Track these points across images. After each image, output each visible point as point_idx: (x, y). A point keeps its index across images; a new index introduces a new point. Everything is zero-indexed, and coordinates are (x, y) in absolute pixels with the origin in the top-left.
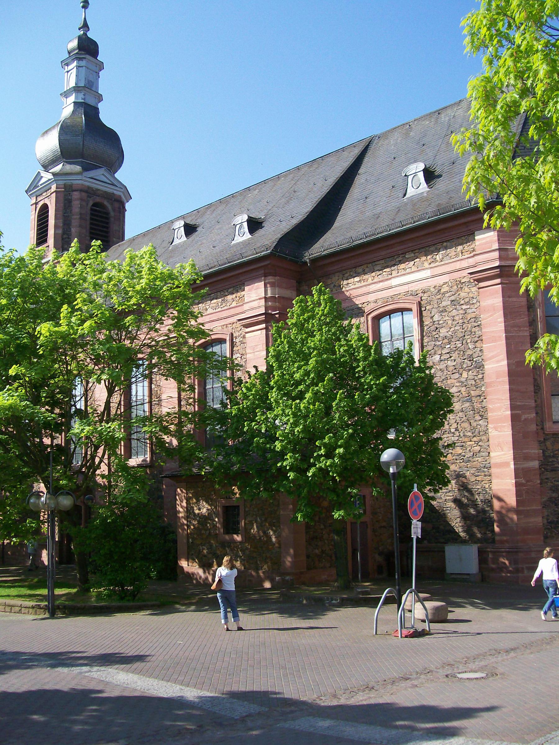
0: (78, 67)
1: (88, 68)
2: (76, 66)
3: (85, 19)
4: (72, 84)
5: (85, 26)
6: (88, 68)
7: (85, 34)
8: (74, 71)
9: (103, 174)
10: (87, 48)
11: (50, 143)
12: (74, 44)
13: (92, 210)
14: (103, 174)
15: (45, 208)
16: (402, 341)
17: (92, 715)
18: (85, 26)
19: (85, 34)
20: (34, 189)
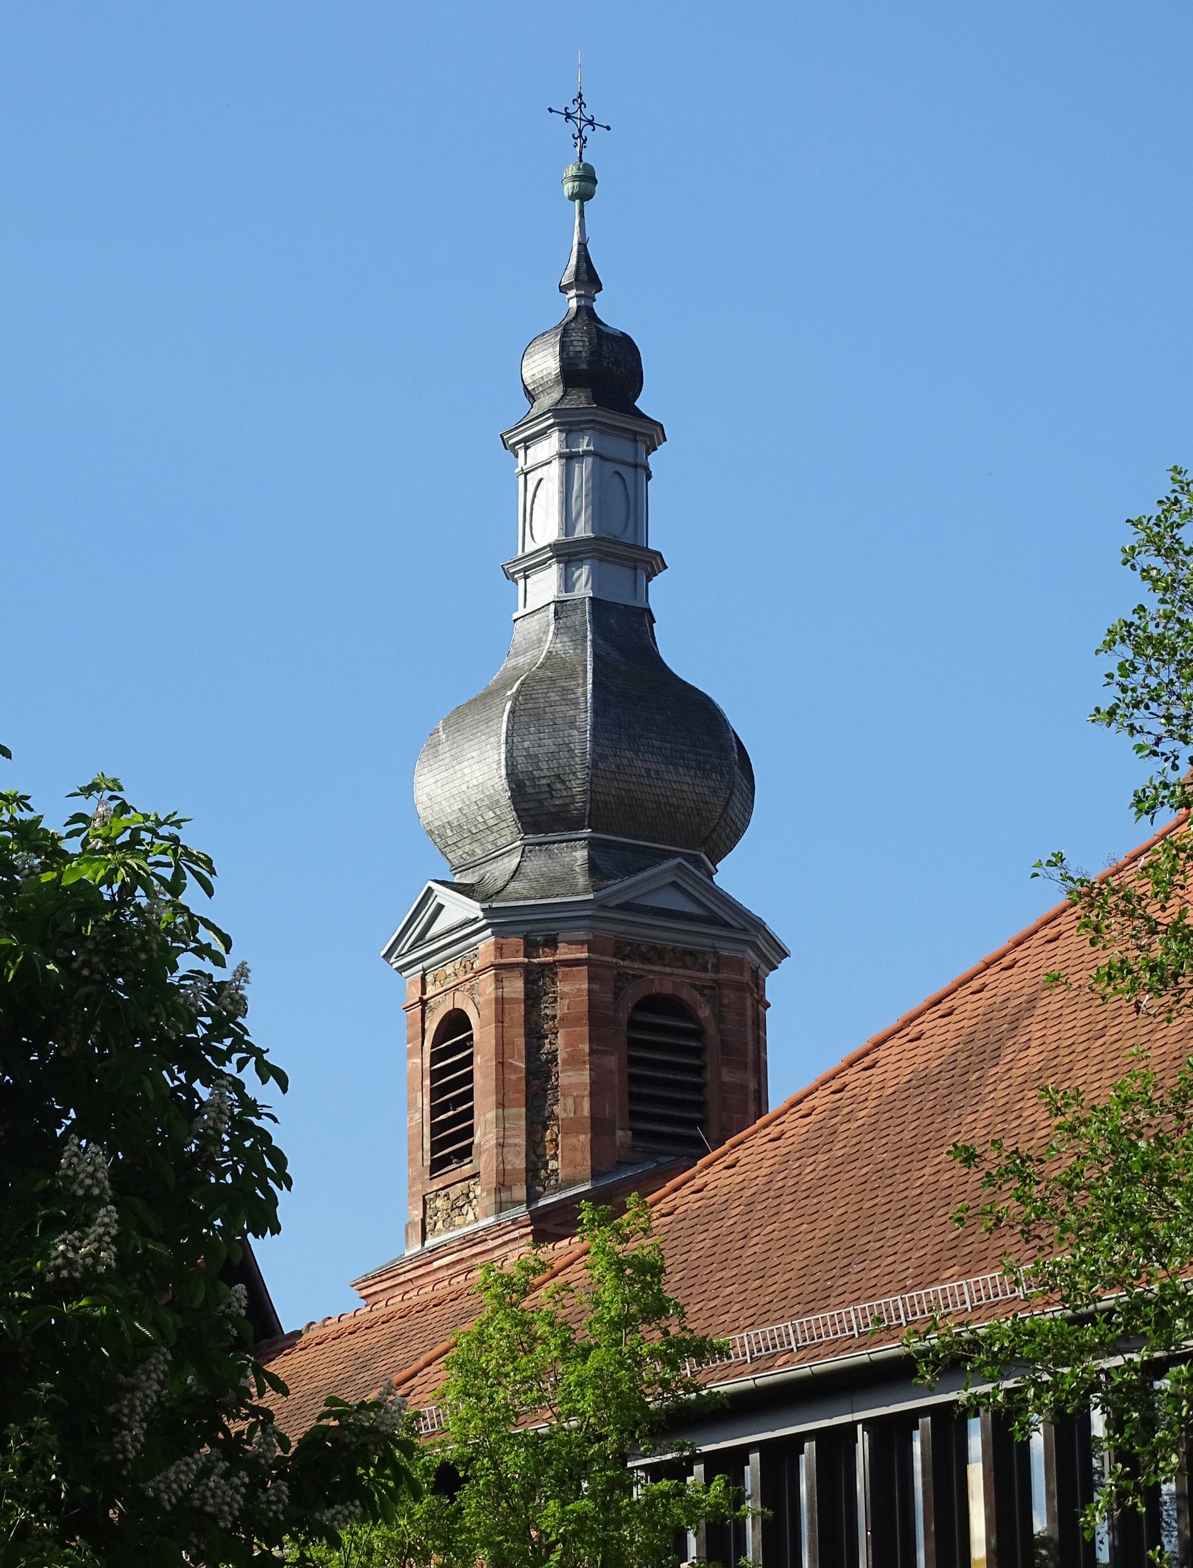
0: (568, 458)
1: (602, 457)
2: (561, 456)
3: (583, 246)
4: (546, 528)
5: (587, 278)
6: (602, 457)
7: (586, 312)
8: (554, 471)
9: (674, 884)
10: (603, 380)
11: (466, 777)
12: (544, 363)
13: (633, 1024)
14: (674, 884)
15: (456, 1022)
16: (631, 460)
17: (602, 954)
18: (587, 278)
19: (586, 312)
20: (415, 937)
